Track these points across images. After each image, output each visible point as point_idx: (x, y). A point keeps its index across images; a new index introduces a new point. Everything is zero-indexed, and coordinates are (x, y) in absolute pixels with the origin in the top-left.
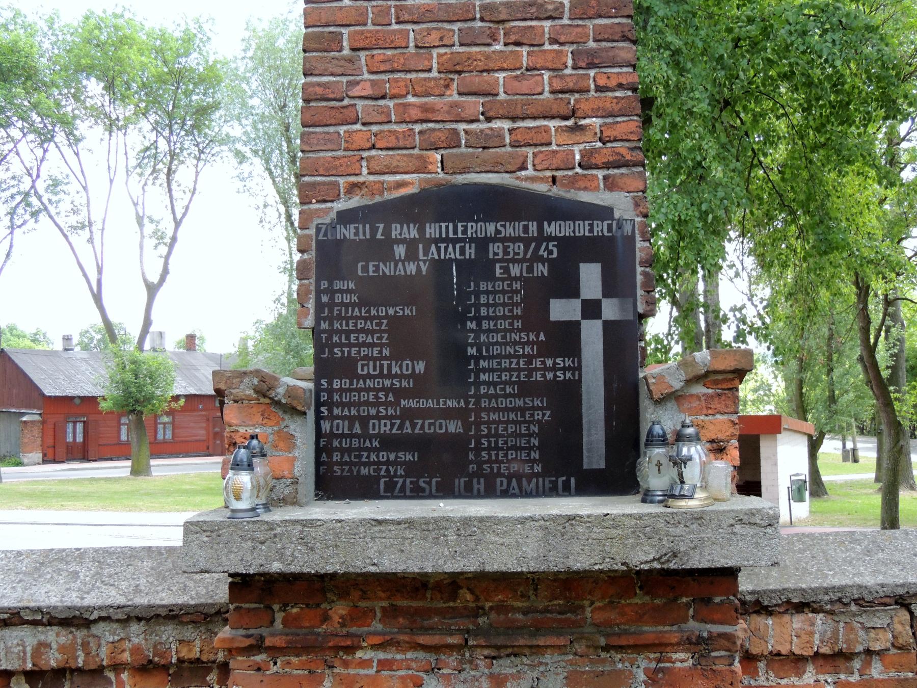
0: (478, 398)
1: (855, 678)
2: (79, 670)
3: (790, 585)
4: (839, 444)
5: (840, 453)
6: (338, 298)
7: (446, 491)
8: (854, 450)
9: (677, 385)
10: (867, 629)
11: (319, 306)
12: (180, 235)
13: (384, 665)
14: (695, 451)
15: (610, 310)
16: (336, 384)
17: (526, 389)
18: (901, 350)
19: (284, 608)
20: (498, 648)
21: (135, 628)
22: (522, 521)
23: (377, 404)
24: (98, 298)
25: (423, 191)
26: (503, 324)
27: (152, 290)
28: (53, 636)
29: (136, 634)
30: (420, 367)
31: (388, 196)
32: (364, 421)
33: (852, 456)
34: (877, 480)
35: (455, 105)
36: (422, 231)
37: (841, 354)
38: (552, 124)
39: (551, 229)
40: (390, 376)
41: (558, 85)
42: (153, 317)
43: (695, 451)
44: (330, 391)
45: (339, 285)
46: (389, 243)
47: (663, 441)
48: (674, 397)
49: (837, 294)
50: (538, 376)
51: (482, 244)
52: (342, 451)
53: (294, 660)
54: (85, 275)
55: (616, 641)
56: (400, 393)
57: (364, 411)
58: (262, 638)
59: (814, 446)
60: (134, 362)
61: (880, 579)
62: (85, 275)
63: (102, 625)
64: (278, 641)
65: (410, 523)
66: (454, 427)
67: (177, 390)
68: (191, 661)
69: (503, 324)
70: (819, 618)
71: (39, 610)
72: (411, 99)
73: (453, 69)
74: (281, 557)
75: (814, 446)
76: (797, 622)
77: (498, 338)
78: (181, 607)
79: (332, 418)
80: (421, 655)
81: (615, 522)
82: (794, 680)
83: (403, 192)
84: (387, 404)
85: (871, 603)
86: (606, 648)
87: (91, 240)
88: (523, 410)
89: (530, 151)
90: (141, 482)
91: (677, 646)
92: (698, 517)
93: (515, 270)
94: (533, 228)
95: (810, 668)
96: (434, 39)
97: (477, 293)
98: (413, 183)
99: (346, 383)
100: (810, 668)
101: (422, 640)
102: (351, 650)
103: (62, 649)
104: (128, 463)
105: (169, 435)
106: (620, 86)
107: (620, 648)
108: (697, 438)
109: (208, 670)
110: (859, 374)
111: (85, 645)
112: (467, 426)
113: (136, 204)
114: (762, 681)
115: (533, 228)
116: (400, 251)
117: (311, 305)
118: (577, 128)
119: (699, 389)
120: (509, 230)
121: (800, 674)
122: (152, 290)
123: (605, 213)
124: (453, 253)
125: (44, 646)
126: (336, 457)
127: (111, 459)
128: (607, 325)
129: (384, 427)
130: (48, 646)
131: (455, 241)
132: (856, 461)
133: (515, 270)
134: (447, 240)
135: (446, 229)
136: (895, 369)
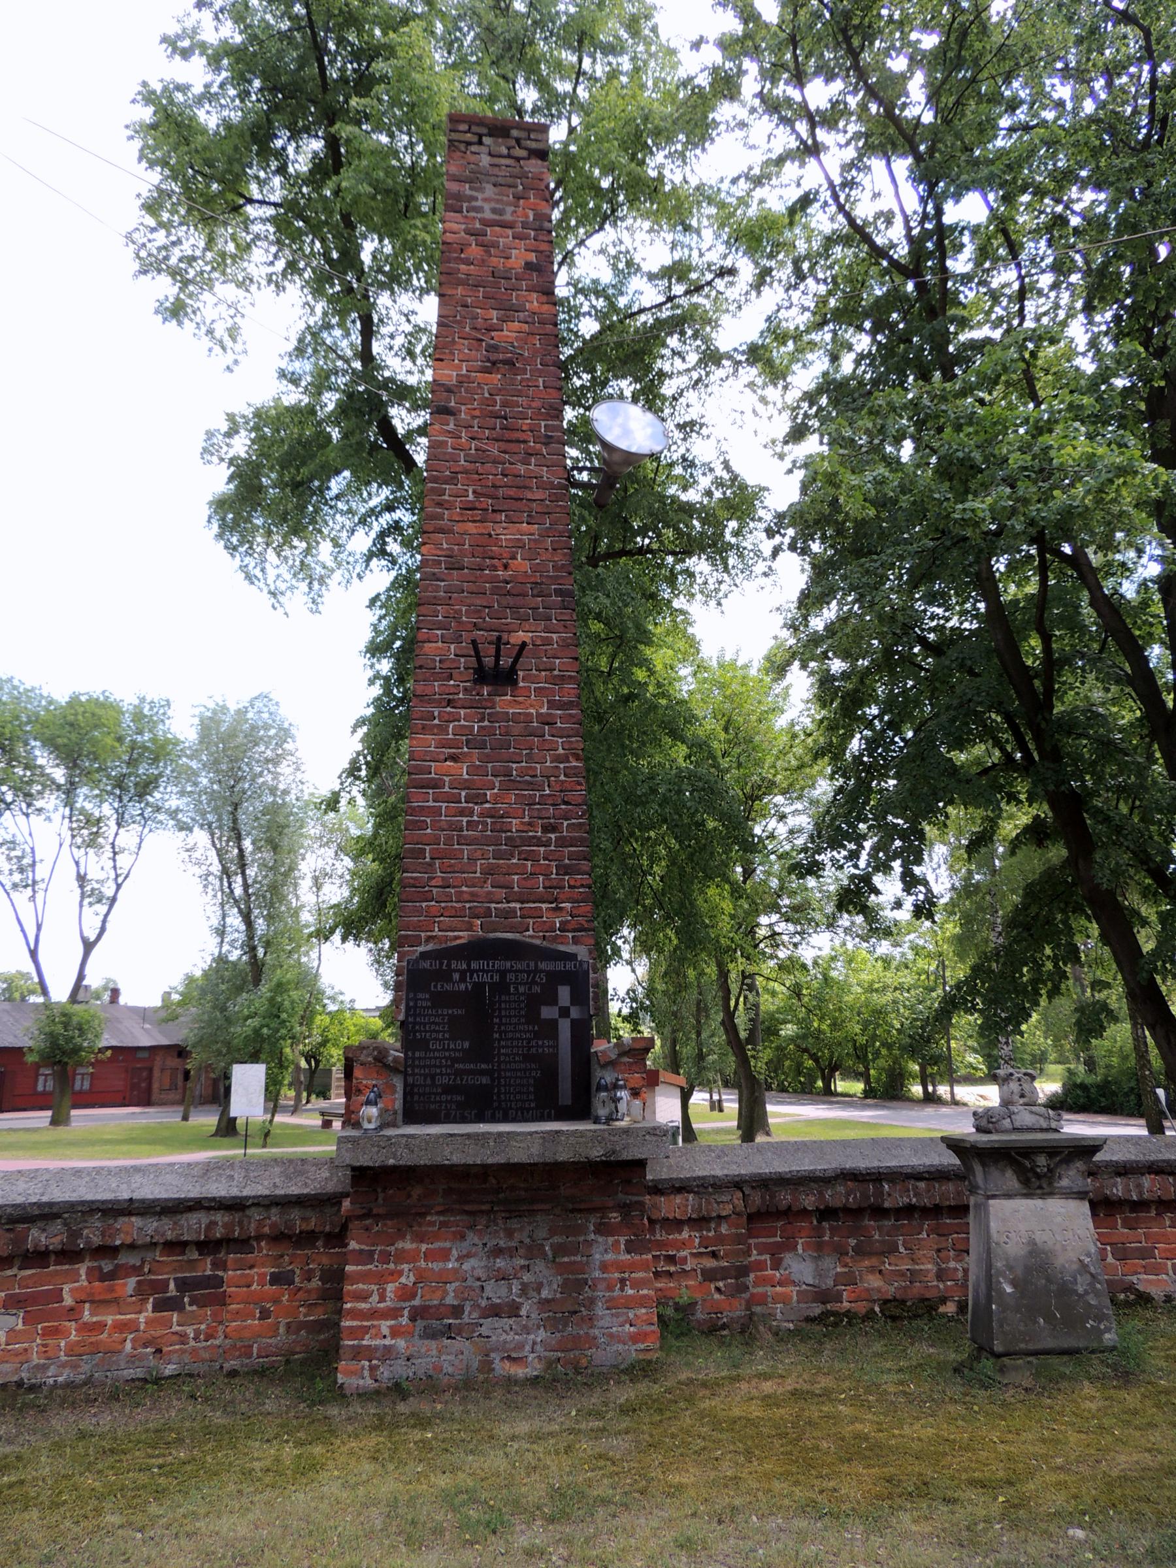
0: (499, 1063)
1: (711, 1234)
2: (236, 1241)
3: (674, 1176)
4: (707, 1096)
5: (707, 1104)
6: (419, 1003)
7: (480, 1119)
8: (720, 1101)
9: (614, 1057)
10: (718, 1203)
11: (408, 1008)
12: (119, 896)
13: (443, 1224)
14: (623, 1094)
15: (575, 1013)
16: (417, 1054)
17: (527, 1058)
18: (757, 1015)
19: (384, 1191)
20: (510, 1211)
21: (274, 1210)
22: (531, 1134)
23: (440, 1067)
24: (34, 954)
25: (469, 943)
26: (514, 1020)
27: (88, 946)
28: (220, 1217)
29: (275, 1215)
30: (466, 1045)
31: (450, 944)
32: (433, 1077)
33: (717, 1106)
34: (739, 1127)
35: (489, 893)
36: (469, 965)
37: (707, 1017)
38: (544, 906)
39: (542, 965)
40: (448, 1050)
41: (547, 884)
42: (87, 971)
43: (623, 1094)
44: (414, 1059)
45: (420, 996)
46: (450, 971)
47: (606, 1088)
48: (612, 1064)
49: (702, 974)
50: (533, 1051)
51: (503, 973)
52: (420, 1095)
53: (389, 1223)
54: (23, 931)
55: (577, 1206)
56: (455, 1060)
57: (433, 1071)
58: (371, 1210)
59: (685, 1097)
60: (64, 1015)
61: (726, 1172)
62: (23, 931)
63: (253, 1209)
64: (381, 1211)
65: (468, 1136)
66: (485, 1080)
67: (103, 1043)
68: (308, 1232)
69: (514, 1020)
70: (691, 1197)
71: (214, 1199)
72: (464, 889)
73: (488, 872)
74: (395, 1157)
75: (685, 1097)
76: (678, 1199)
77: (511, 1028)
78: (306, 1195)
79: (414, 1074)
80: (465, 1217)
81: (582, 1134)
82: (677, 1236)
83: (458, 942)
84: (446, 1066)
85: (720, 1187)
86: (572, 1211)
87: (33, 898)
88: (525, 1070)
89: (531, 921)
90: (61, 1132)
91: (612, 1209)
92: (626, 1131)
93: (521, 989)
94: (532, 964)
95: (686, 1228)
96: (478, 854)
97: (500, 1002)
98: (464, 936)
99: (423, 1054)
100: (686, 1228)
101: (467, 1208)
102: (423, 1215)
103: (225, 1225)
104: (49, 1113)
105: (86, 1085)
106: (582, 886)
107: (580, 1211)
108: (624, 1087)
109: (317, 1239)
110: (721, 1037)
111: (240, 1223)
112: (493, 1080)
113: (77, 863)
114: (658, 1237)
115: (532, 964)
116: (456, 976)
117: (403, 1007)
118: (558, 909)
119: (626, 1059)
120: (518, 966)
121: (680, 1232)
122: (88, 946)
123: (572, 957)
124: (486, 978)
125: (213, 1224)
126: (416, 1098)
127: (25, 1110)
128: (573, 1021)
129: (445, 1080)
130: (216, 1223)
131: (487, 972)
132: (721, 1110)
133: (521, 989)
134: (483, 971)
135: (483, 964)
136: (752, 1032)
